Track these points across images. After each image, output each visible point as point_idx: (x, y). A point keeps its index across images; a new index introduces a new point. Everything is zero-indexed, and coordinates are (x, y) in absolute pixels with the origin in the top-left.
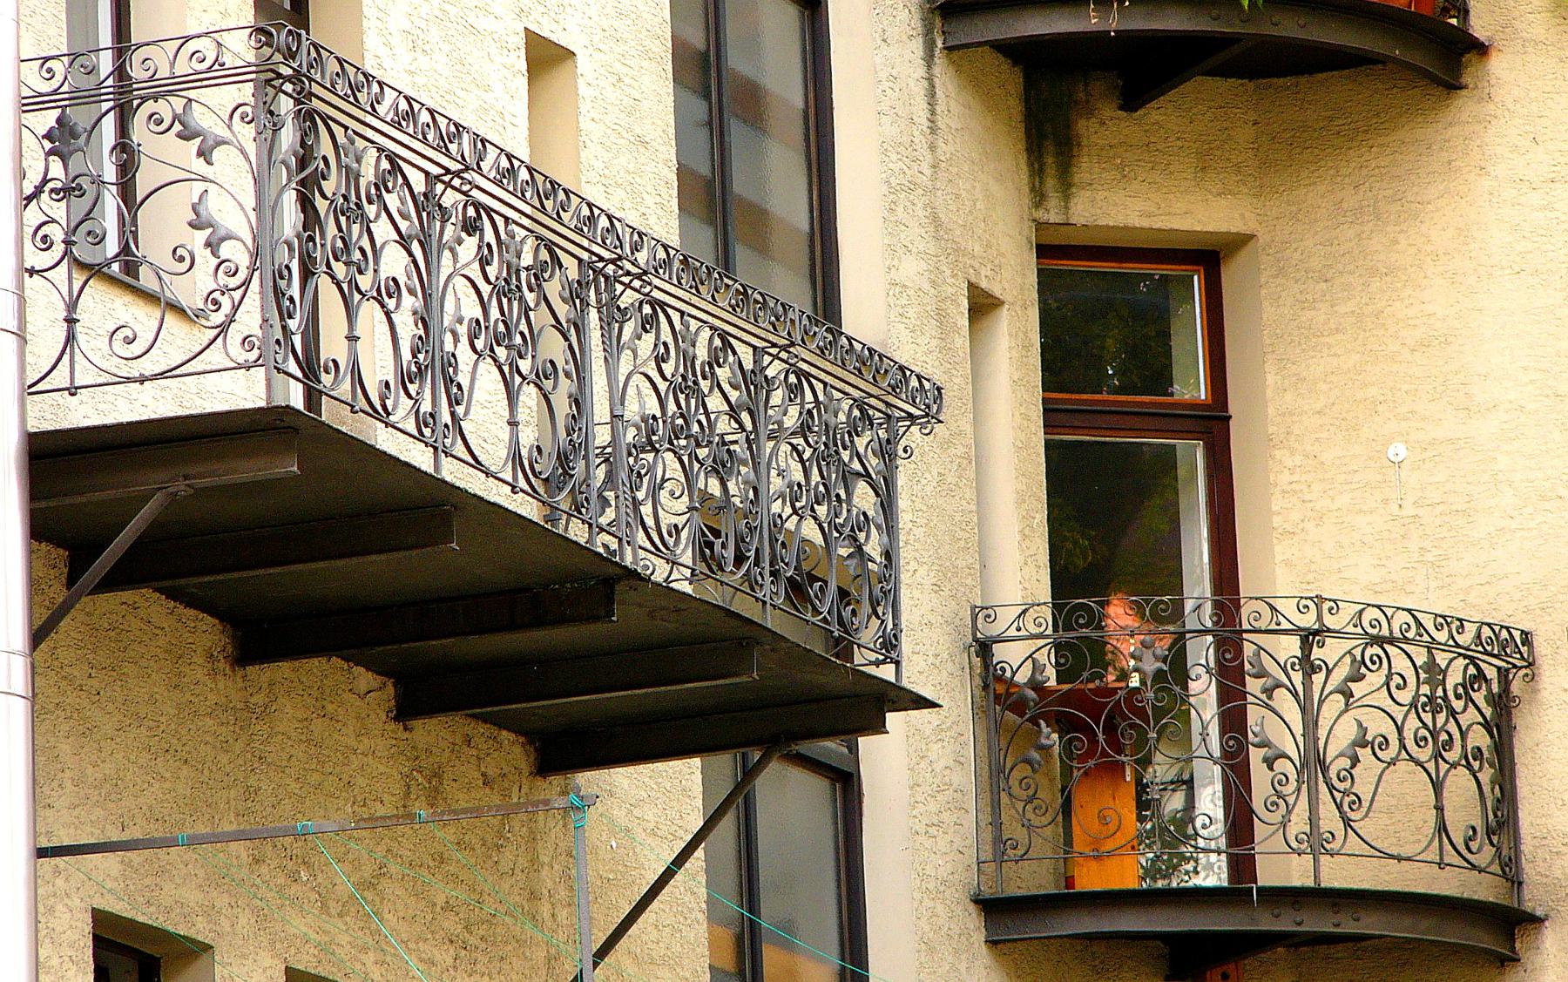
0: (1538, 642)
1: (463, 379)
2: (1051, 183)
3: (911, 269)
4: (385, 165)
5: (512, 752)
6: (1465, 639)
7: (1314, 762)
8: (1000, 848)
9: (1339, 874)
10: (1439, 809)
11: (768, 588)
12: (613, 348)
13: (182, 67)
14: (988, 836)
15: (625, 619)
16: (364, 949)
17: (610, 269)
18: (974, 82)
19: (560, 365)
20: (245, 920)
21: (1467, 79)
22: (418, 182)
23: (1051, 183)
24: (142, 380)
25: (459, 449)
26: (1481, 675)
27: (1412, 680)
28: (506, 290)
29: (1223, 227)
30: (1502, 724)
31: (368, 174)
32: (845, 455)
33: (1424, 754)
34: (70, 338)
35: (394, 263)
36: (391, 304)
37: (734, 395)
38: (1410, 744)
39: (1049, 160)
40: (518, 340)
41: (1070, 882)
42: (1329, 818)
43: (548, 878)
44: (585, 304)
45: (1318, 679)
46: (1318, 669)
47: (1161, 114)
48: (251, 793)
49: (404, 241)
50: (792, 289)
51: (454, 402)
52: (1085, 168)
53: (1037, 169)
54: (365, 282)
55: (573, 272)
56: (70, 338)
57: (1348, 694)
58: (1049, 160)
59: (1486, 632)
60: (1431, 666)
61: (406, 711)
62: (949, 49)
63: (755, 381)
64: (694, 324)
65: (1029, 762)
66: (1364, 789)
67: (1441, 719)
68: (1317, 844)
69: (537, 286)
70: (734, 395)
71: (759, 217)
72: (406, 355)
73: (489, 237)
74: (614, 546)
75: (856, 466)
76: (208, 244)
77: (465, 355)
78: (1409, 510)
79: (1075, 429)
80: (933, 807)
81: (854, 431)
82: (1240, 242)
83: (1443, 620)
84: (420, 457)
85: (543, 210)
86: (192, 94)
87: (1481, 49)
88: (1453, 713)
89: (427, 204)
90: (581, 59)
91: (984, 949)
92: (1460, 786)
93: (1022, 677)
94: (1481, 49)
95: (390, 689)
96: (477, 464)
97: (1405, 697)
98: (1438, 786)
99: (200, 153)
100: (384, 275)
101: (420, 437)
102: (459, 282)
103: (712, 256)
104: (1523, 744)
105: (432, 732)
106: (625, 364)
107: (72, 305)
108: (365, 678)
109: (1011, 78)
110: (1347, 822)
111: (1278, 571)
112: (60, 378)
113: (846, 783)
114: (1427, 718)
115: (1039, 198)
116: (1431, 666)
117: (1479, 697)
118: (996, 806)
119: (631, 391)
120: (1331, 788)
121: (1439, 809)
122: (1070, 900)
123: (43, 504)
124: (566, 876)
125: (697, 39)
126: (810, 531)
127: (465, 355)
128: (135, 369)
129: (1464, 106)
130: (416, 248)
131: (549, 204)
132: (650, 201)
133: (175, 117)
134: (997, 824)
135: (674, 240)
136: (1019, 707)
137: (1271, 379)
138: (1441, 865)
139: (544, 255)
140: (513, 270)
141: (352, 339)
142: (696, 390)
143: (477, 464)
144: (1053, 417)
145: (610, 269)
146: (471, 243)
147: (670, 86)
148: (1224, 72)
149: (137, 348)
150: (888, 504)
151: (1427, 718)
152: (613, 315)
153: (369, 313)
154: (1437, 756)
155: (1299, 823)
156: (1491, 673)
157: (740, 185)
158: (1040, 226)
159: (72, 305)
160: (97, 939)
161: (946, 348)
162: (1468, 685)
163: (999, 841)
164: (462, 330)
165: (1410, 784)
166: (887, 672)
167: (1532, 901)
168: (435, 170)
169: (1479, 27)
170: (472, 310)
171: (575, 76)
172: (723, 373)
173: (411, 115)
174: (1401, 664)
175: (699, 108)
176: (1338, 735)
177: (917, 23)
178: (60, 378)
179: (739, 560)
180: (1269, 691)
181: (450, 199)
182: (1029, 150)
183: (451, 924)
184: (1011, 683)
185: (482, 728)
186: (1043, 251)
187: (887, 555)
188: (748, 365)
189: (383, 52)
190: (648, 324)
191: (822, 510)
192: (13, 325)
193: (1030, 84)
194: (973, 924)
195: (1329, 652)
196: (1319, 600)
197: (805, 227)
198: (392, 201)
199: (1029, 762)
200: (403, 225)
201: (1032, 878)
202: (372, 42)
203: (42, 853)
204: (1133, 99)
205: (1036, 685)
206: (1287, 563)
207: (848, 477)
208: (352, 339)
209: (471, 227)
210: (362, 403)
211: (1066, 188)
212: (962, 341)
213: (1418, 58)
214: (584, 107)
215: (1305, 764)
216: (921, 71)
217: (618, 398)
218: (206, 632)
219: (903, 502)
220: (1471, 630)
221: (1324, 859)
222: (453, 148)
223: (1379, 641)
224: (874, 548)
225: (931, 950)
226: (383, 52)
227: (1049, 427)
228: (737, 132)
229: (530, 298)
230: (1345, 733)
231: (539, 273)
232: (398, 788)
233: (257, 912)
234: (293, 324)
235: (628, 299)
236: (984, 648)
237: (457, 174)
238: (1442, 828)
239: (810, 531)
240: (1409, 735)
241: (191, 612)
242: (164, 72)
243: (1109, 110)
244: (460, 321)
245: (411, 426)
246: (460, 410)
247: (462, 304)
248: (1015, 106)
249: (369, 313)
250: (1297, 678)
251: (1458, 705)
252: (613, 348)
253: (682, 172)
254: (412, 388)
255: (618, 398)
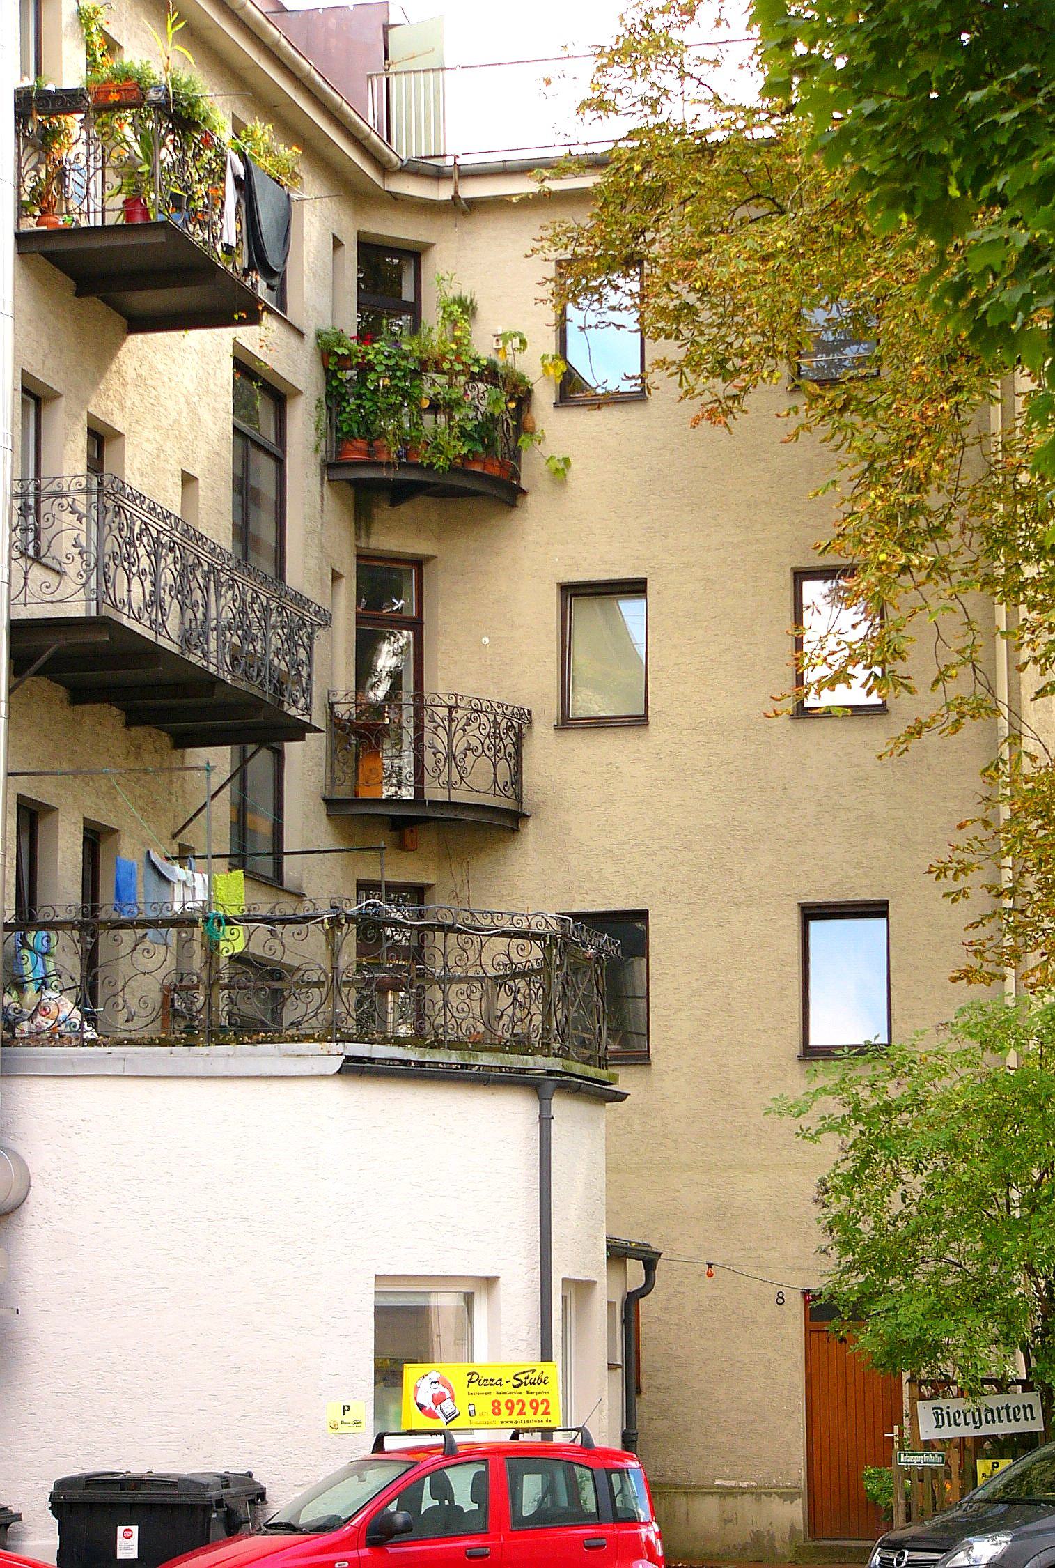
0: (533, 714)
1: (111, 573)
2: (363, 532)
3: (312, 563)
4: (143, 526)
5: (165, 740)
6: (508, 712)
7: (450, 755)
8: (333, 781)
9: (458, 797)
10: (495, 774)
11: (267, 687)
12: (218, 595)
13: (73, 487)
14: (329, 775)
15: (218, 695)
16: (111, 811)
17: (219, 567)
18: (336, 492)
19: (200, 602)
20: (70, 800)
21: (519, 503)
22: (154, 534)
23: (363, 532)
24: (52, 602)
25: (164, 633)
26: (512, 726)
27: (488, 726)
28: (182, 574)
29: (425, 552)
30: (518, 745)
31: (137, 530)
32: (296, 638)
33: (491, 754)
34: (25, 584)
35: (145, 563)
36: (143, 578)
37: (259, 615)
38: (486, 750)
39: (363, 523)
40: (186, 593)
41: (356, 794)
42: (455, 776)
43: (175, 787)
44: (209, 580)
45: (454, 724)
46: (453, 721)
47: (405, 509)
48: (74, 752)
49: (148, 555)
50: (268, 569)
51: (163, 615)
52: (376, 527)
53: (358, 528)
54: (134, 570)
55: (206, 568)
56: (25, 584)
57: (464, 731)
58: (363, 523)
59: (515, 710)
60: (495, 721)
61: (129, 724)
62: (329, 480)
63: (266, 610)
64: (247, 588)
65: (346, 749)
66: (468, 765)
67: (497, 741)
68: (450, 785)
69: (193, 573)
70: (259, 615)
71: (257, 540)
72: (148, 598)
73: (178, 555)
74: (205, 664)
75: (300, 642)
76: (80, 554)
77: (167, 598)
78: (489, 662)
79: (373, 625)
80: (310, 764)
81: (300, 629)
82: (430, 558)
83: (501, 705)
84: (149, 634)
85: (198, 545)
86: (76, 497)
87: (524, 493)
88: (502, 739)
89: (157, 541)
90: (201, 483)
91: (325, 817)
92: (502, 765)
93: (346, 717)
94: (524, 493)
95: (124, 715)
96: (170, 639)
97: (485, 732)
98: (495, 766)
99: (78, 519)
100: (141, 567)
101: (151, 628)
102: (167, 571)
103: (274, 572)
104: (525, 752)
105: (137, 732)
106: (222, 601)
107: (26, 573)
108: (115, 711)
109: (350, 492)
110: (461, 777)
111: (439, 682)
112: (21, 598)
113: (279, 756)
114: (492, 740)
115: (358, 537)
116: (495, 721)
117: (511, 734)
118: (332, 764)
119: (224, 613)
120: (457, 765)
121: (495, 774)
122: (356, 801)
123: (16, 645)
124: (181, 786)
125: (240, 474)
126: (283, 666)
127: (167, 598)
128: (49, 598)
129: (517, 513)
130: (152, 557)
131: (200, 543)
132: (222, 535)
133: (69, 505)
134: (332, 771)
135: (230, 551)
136: (343, 728)
137: (440, 610)
138: (494, 795)
139: (196, 561)
140: (185, 566)
141: (129, 591)
142: (246, 613)
143: (170, 639)
144: (360, 618)
145: (219, 567)
146: (171, 556)
147: (230, 493)
148: (428, 495)
149: (50, 590)
150: (310, 657)
151: (492, 740)
152: (218, 583)
153: (136, 580)
154: (495, 755)
155: (444, 778)
156: (516, 725)
157: (252, 528)
158: (357, 548)
159: (26, 573)
160: (18, 805)
161: (324, 593)
162: (508, 728)
163: (333, 778)
164: (167, 588)
165: (485, 764)
166: (306, 719)
167: (526, 809)
168: (161, 529)
169: (524, 485)
170: (171, 581)
171: (197, 487)
172: (256, 606)
173: (154, 509)
174: (484, 720)
175: (239, 498)
176: (460, 745)
177: (318, 470)
178: (21, 598)
179: (258, 675)
180: (436, 728)
181: (165, 539)
182: (355, 519)
183: (141, 802)
184: (341, 720)
185: (156, 731)
186: (358, 557)
187: (309, 676)
188: (265, 604)
189: (131, 476)
190: (231, 587)
191: (287, 658)
192: (6, 579)
193: (356, 491)
194: (322, 807)
195: (458, 714)
196: (456, 695)
197: (274, 545)
198: (145, 539)
199: (346, 749)
200: (149, 549)
201: (343, 792)
202: (127, 472)
203: (9, 774)
204: (394, 503)
205: (349, 720)
206: (442, 679)
207: (297, 645)
208: (129, 591)
209: (172, 550)
210: (132, 615)
211: (368, 534)
212: (329, 591)
213: (502, 495)
214: (201, 499)
215: (448, 756)
216: (319, 489)
217: (219, 615)
218: (60, 692)
219: (315, 657)
220: (510, 709)
221: (452, 791)
222: (168, 521)
223: (477, 711)
224: (304, 673)
225: (307, 817)
226: (131, 476)
227: (357, 624)
228: (252, 508)
229: (191, 577)
230: (462, 745)
231: (194, 567)
232: (125, 752)
233: (74, 796)
234: (109, 585)
235: (224, 578)
236: (332, 706)
237: (113, 494)
238: (495, 782)
239: (283, 666)
240: (485, 746)
241: (56, 685)
242: (66, 489)
243: (385, 506)
244: (166, 585)
245: (148, 623)
246: (165, 618)
247: (168, 578)
248: (351, 503)
249: (136, 580)
250: (447, 723)
251: (503, 736)
252: (218, 595)
253: (234, 524)
254: (149, 609)
255: (219, 615)
